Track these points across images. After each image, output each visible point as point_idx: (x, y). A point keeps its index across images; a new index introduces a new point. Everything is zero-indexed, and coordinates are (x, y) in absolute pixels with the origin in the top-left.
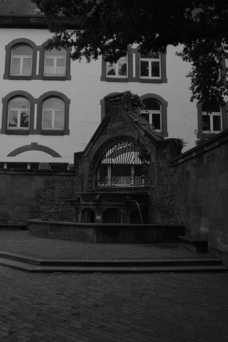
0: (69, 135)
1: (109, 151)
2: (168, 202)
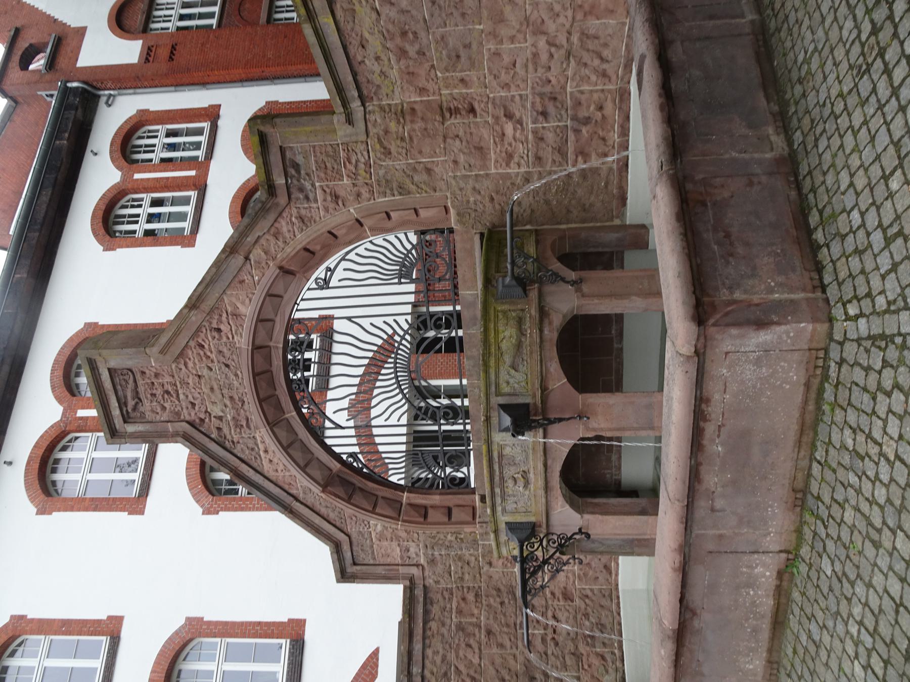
0: (305, 621)
1: (337, 450)
2: (515, 129)
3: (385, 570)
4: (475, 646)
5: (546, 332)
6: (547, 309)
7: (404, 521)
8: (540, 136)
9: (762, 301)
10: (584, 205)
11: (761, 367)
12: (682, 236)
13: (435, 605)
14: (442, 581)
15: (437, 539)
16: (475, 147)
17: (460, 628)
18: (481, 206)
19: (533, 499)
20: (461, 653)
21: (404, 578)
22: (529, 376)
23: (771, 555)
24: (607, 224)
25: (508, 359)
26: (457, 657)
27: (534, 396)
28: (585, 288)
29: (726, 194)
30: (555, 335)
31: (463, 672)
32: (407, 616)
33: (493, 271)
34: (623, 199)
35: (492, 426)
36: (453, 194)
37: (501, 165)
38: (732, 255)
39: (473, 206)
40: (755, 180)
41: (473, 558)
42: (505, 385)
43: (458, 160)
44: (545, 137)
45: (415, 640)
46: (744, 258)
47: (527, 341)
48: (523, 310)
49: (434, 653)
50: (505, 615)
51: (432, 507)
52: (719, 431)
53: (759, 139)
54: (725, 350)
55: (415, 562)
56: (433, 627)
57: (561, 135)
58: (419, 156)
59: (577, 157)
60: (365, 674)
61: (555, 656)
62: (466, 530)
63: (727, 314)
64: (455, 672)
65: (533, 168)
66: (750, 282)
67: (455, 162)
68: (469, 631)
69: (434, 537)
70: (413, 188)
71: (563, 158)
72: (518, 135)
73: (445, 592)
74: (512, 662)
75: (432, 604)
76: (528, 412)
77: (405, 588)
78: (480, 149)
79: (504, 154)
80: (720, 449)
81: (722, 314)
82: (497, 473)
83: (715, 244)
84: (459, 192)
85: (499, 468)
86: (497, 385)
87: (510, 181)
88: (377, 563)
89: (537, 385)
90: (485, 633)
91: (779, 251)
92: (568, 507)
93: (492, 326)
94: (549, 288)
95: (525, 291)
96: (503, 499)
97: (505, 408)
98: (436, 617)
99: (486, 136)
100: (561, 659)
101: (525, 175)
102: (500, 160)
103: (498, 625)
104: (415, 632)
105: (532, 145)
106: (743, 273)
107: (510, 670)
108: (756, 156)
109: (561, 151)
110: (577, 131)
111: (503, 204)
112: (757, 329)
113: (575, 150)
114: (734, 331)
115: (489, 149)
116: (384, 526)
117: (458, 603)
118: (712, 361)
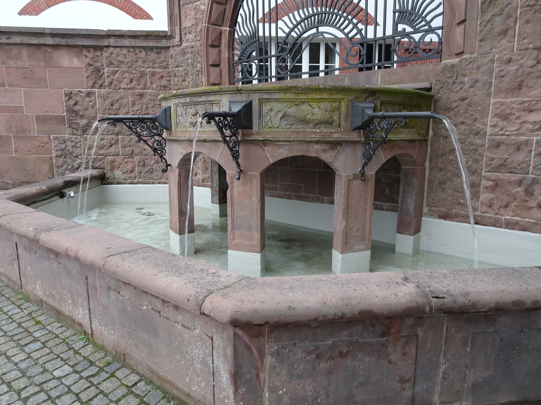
3: (176, 15)
4: (132, 85)
5: (316, 146)
6: (339, 148)
7: (208, 28)
8: (522, 147)
9: (262, 381)
10: (445, 184)
11: (201, 364)
12: (340, 315)
13: (156, 55)
14: (173, 60)
15: (198, 56)
16: (523, 81)
17: (143, 75)
18: (458, 89)
19: (184, 129)
20: (126, 75)
21: (172, 30)
22: (276, 130)
23: (89, 323)
24: (425, 202)
25: (292, 110)
26: (123, 72)
27: (258, 134)
28: (357, 183)
29: (393, 357)
30: (313, 154)
31: (114, 76)
32: (147, 33)
33: (383, 98)
34: (445, 217)
35: (233, 95)
36: (475, 60)
37: (497, 108)
38: (318, 357)
39: (459, 80)
40: (407, 386)
41: (187, 84)
42: (269, 107)
43: (511, 64)
44: (520, 152)
45: (132, 40)
46: (314, 369)
47: (308, 129)
48: (339, 125)
49: (125, 55)
50: (153, 107)
51: (220, 51)
52: (156, 311)
53: (458, 392)
54: (214, 338)
55: (183, 39)
56: (141, 54)
57: (520, 168)
58: (523, 20)
59: (493, 181)
60: (135, 10)
61: (130, 140)
62: (204, 78)
63: (249, 348)
64: (114, 71)
65: (488, 139)
66: (284, 373)
67: (509, 61)
68: (141, 81)
69: (198, 53)
70: (488, 16)
71: (493, 168)
72: (527, 125)
73: (165, 63)
74: (124, 111)
75: (157, 53)
76: (246, 128)
77: (166, 32)
78: (519, 87)
79: (508, 111)
80: (145, 307)
81: (249, 343)
82: (199, 100)
83: (333, 342)
84: (475, 65)
85: (203, 101)
86: (269, 100)
87: (479, 117)
88: (181, 8)
89: (268, 137)
90: (140, 92)
91: (319, 400)
92: (181, 157)
93: (325, 96)
94: (359, 151)
95: (359, 128)
96: (184, 104)
97: (248, 107)
98: (148, 57)
99: (532, 93)
100: (129, 144)
101: (482, 132)
102: (503, 107)
103: (146, 102)
104: (137, 40)
105: (513, 140)
106: (295, 366)
107: (119, 109)
108: (438, 388)
109: (501, 167)
110: (520, 183)
111: (457, 109)
112: (230, 373)
113: (500, 180)
114: (230, 351)
115: (517, 96)
116: (204, 12)
117: (159, 73)
118: (206, 323)
